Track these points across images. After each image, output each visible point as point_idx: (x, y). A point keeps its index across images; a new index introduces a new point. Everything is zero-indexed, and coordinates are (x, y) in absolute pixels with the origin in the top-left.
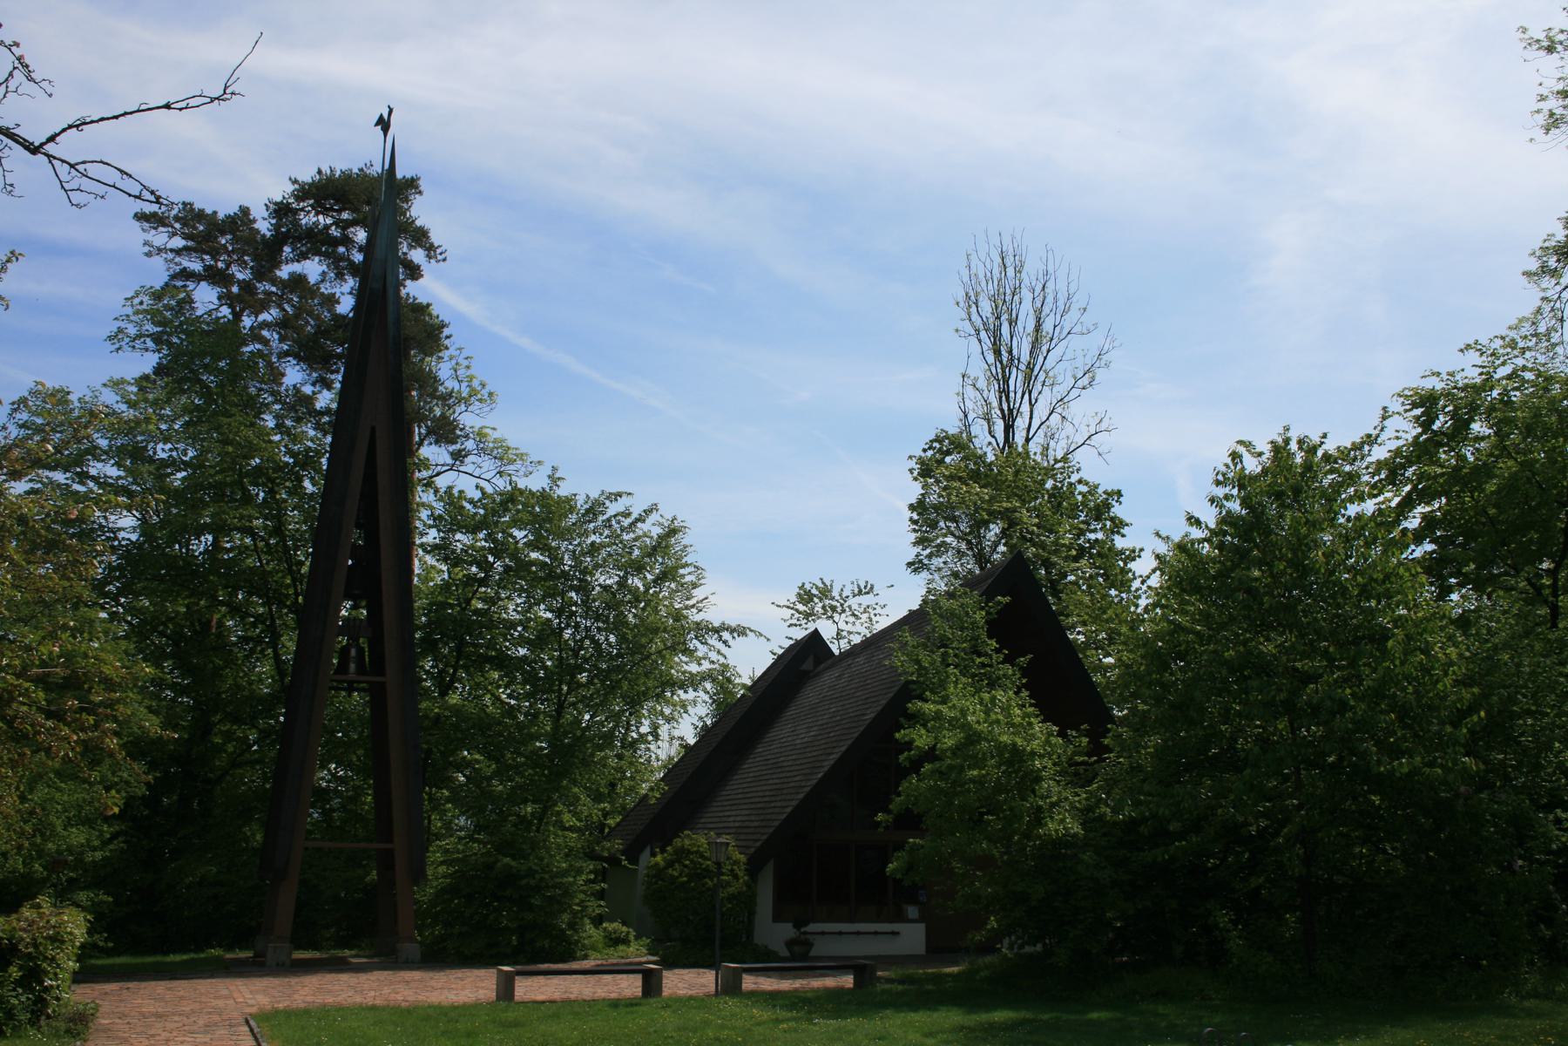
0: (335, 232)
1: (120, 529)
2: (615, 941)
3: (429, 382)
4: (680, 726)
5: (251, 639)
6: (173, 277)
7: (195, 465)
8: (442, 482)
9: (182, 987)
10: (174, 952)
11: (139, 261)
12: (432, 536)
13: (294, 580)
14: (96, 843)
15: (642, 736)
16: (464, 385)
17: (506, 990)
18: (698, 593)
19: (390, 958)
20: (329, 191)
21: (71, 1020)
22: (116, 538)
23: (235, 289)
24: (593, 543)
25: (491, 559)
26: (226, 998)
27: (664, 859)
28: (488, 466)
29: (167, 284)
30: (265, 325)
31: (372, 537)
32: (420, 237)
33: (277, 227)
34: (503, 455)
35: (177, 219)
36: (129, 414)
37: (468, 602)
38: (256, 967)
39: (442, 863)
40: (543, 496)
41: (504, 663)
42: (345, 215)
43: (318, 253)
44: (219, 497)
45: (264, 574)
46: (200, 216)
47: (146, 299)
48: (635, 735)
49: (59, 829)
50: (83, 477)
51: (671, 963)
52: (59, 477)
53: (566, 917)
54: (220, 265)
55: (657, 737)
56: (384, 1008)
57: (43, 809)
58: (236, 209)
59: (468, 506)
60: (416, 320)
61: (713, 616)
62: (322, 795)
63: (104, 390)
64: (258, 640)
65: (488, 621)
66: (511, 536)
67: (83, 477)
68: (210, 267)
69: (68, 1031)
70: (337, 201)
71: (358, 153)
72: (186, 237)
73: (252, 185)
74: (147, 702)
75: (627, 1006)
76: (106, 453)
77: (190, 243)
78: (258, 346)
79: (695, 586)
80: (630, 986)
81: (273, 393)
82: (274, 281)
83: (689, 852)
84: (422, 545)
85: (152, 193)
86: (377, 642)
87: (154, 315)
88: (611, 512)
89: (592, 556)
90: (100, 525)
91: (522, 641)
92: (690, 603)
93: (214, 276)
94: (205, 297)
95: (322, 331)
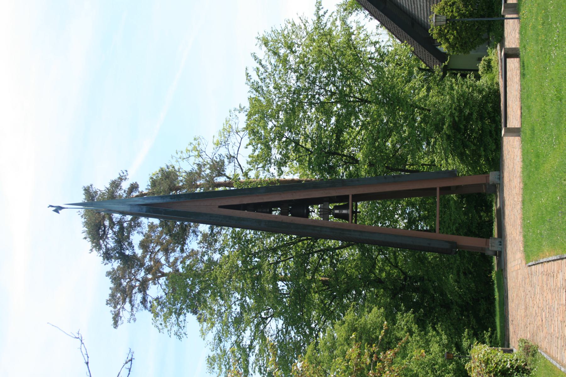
0: (116, 228)
1: (277, 328)
2: (489, 67)
3: (192, 177)
4: (372, 32)
5: (331, 261)
6: (146, 307)
7: (243, 292)
8: (246, 167)
9: (512, 294)
10: (494, 295)
11: (141, 324)
12: (273, 169)
13: (300, 241)
14: (438, 338)
15: (377, 51)
16: (191, 154)
17: (515, 132)
18: (298, 22)
19: (497, 188)
20: (96, 232)
21: (527, 354)
22: (282, 330)
23: (150, 276)
24: (275, 88)
25: (284, 139)
26: (517, 274)
27: (444, 43)
28: (234, 139)
29: (150, 311)
30: (167, 260)
31: (276, 204)
32: (116, 185)
33: (116, 258)
34: (228, 131)
35: (115, 307)
36: (218, 326)
37: (308, 150)
38: (501, 255)
39: (447, 160)
40: (250, 115)
41: (339, 131)
42: (107, 223)
43: (128, 237)
44: (258, 278)
45: (298, 255)
46: (113, 296)
47: (159, 322)
48: (376, 54)
49: (431, 357)
50: (251, 347)
51: (501, 39)
52: (252, 359)
53: (476, 94)
54: (138, 284)
55: (377, 42)
56: (523, 197)
57: (421, 364)
58: (108, 278)
59: (257, 153)
60: (160, 184)
61: (312, 18)
62: (412, 222)
63: (206, 340)
64: (332, 257)
65: (317, 141)
66: (271, 129)
67: (251, 347)
68: (139, 289)
69: (533, 355)
70: (100, 228)
71: (76, 222)
72: (124, 302)
73: (94, 271)
74: (366, 313)
75: (524, 69)
76: (238, 337)
77: (128, 300)
78: (179, 263)
79: (294, 25)
80: (513, 64)
81: (203, 255)
82: (144, 257)
83: (440, 30)
84: (280, 175)
85: (126, 363)
86: (331, 200)
87: (166, 317)
88: (257, 79)
89: (281, 88)
90: (276, 338)
91: (328, 121)
92: (303, 27)
93: (144, 287)
94: (155, 291)
95: (169, 232)
